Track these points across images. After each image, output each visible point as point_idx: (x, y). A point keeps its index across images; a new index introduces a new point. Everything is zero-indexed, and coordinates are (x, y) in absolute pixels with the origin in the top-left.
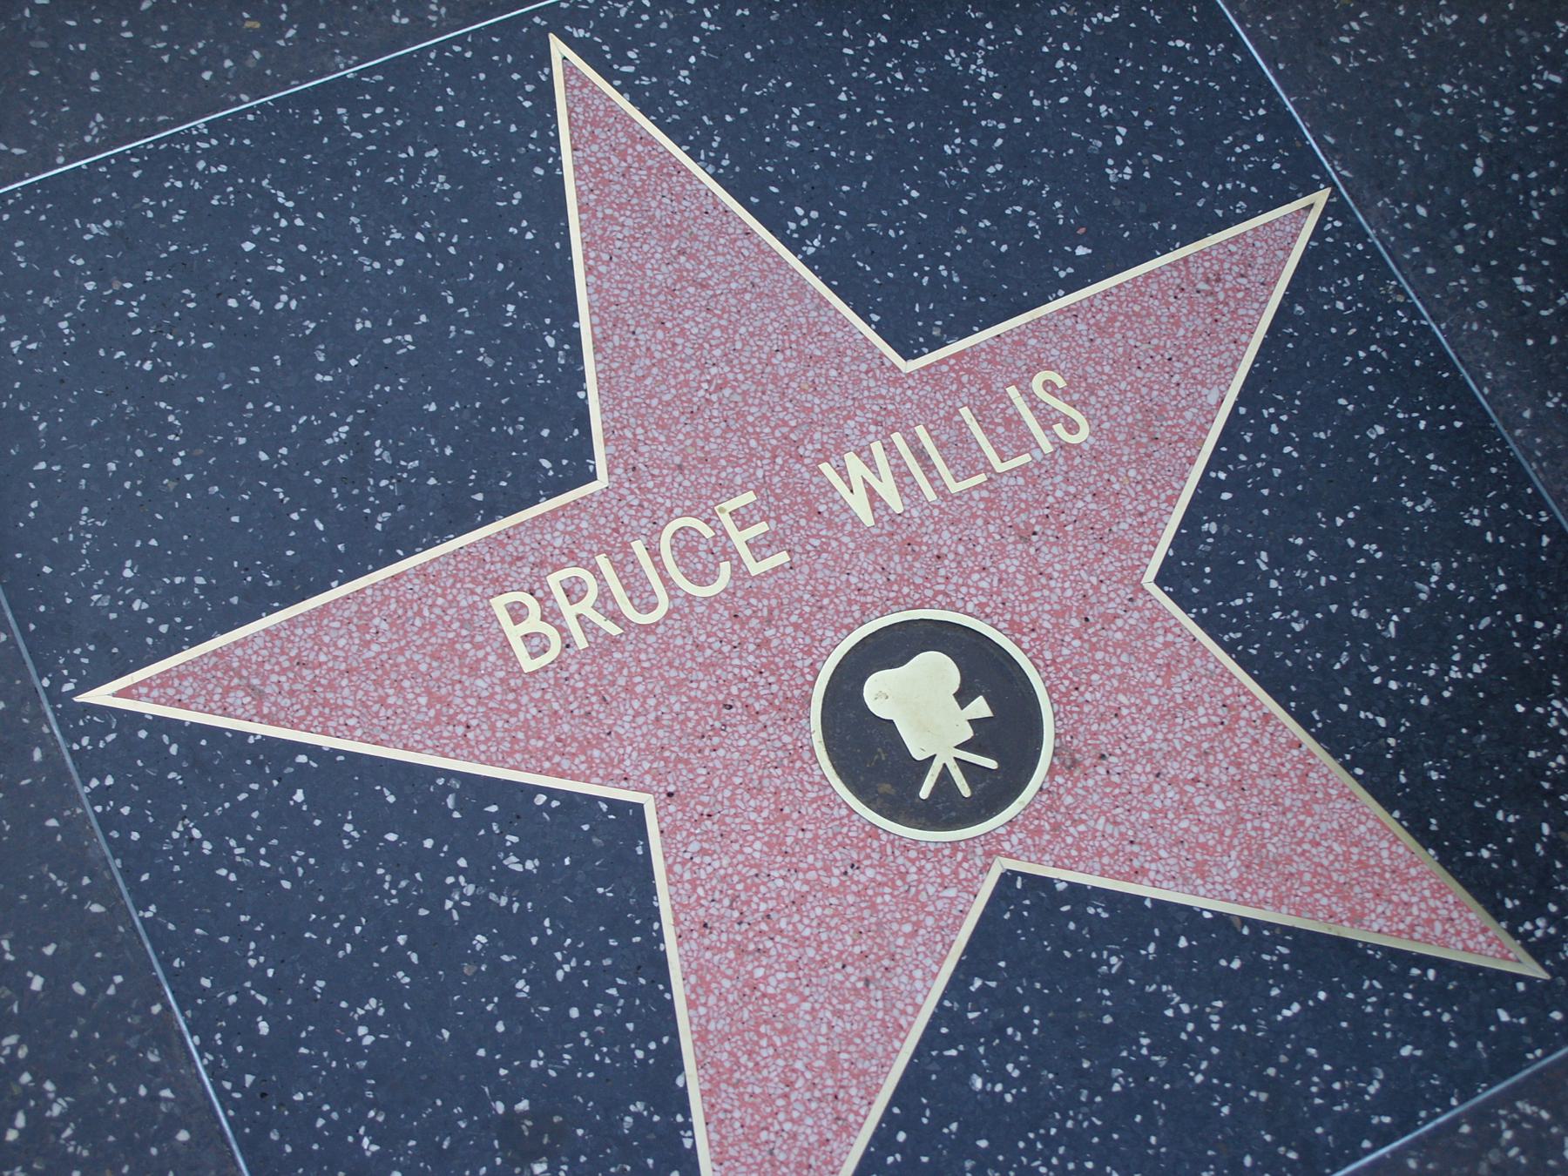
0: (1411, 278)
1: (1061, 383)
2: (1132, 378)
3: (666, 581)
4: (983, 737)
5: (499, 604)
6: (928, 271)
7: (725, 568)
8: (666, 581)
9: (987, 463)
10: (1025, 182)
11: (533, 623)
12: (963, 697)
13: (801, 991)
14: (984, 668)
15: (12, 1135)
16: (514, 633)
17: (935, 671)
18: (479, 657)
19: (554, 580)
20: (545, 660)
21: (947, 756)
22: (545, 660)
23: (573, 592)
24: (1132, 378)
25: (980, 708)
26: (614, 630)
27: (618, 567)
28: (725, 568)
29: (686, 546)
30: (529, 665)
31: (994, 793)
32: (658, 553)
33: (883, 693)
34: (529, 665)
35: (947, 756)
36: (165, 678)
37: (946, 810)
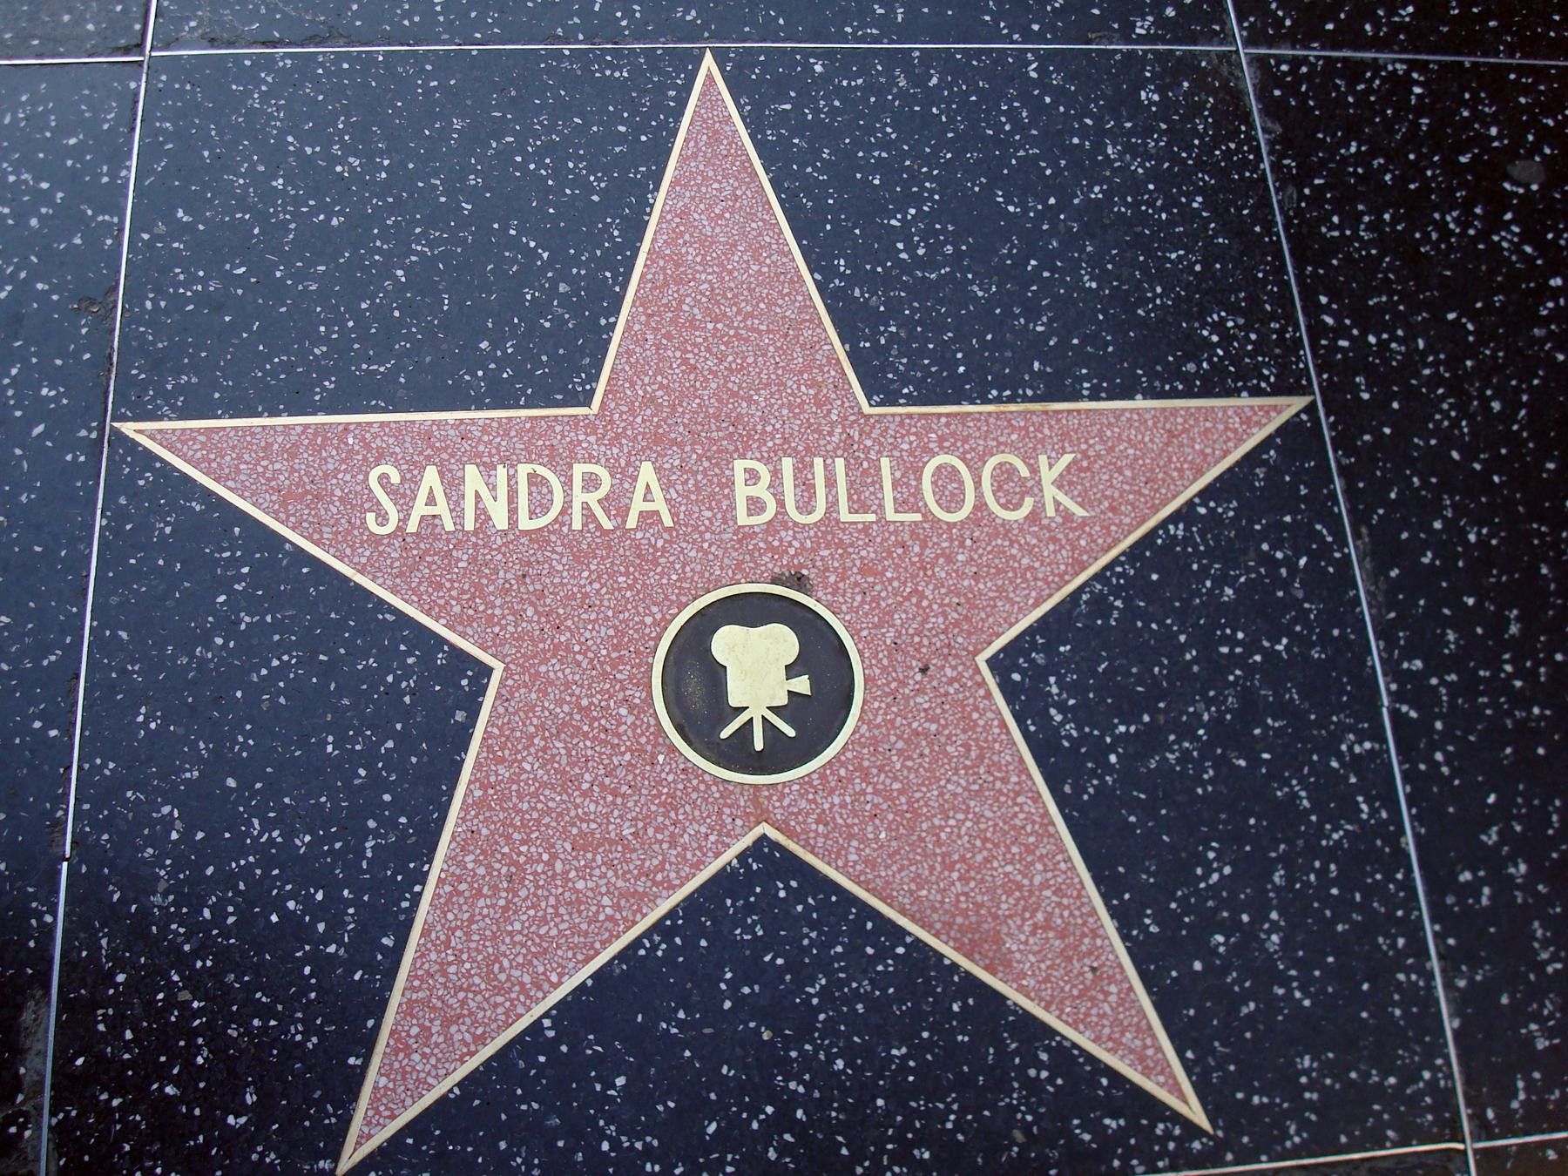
0: (1373, 1163)
1: (395, 478)
2: (1068, 484)
3: (978, 484)
4: (794, 707)
5: (740, 466)
6: (930, 331)
7: (1029, 503)
8: (978, 484)
9: (881, 506)
10: (180, 213)
11: (761, 491)
12: (791, 671)
13: (491, 951)
14: (821, 655)
15: (1413, 714)
16: (742, 492)
17: (781, 642)
18: (414, 501)
19: (579, 470)
20: (754, 520)
21: (756, 712)
22: (754, 520)
23: (591, 483)
24: (1068, 484)
25: (802, 685)
26: (607, 524)
27: (797, 471)
28: (1029, 503)
29: (1005, 475)
30: (743, 519)
31: (781, 754)
32: (563, 512)
33: (728, 643)
34: (743, 519)
35: (756, 712)
36: (186, 436)
37: (738, 754)
